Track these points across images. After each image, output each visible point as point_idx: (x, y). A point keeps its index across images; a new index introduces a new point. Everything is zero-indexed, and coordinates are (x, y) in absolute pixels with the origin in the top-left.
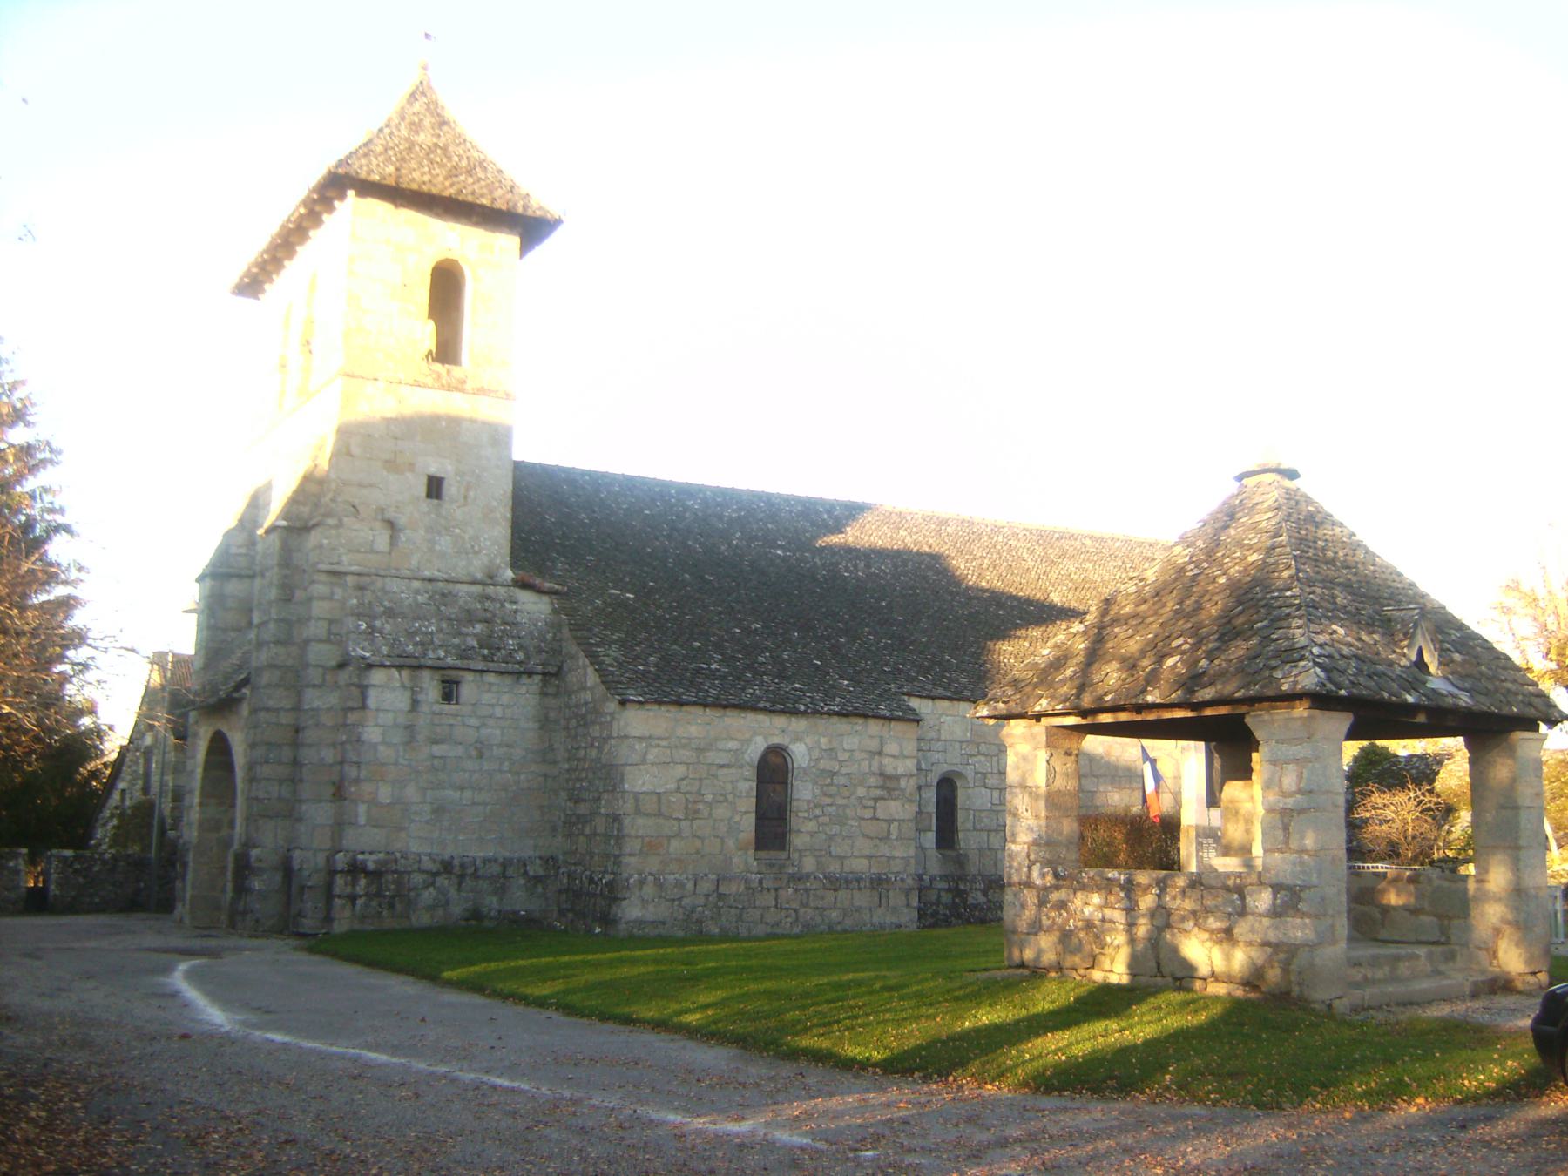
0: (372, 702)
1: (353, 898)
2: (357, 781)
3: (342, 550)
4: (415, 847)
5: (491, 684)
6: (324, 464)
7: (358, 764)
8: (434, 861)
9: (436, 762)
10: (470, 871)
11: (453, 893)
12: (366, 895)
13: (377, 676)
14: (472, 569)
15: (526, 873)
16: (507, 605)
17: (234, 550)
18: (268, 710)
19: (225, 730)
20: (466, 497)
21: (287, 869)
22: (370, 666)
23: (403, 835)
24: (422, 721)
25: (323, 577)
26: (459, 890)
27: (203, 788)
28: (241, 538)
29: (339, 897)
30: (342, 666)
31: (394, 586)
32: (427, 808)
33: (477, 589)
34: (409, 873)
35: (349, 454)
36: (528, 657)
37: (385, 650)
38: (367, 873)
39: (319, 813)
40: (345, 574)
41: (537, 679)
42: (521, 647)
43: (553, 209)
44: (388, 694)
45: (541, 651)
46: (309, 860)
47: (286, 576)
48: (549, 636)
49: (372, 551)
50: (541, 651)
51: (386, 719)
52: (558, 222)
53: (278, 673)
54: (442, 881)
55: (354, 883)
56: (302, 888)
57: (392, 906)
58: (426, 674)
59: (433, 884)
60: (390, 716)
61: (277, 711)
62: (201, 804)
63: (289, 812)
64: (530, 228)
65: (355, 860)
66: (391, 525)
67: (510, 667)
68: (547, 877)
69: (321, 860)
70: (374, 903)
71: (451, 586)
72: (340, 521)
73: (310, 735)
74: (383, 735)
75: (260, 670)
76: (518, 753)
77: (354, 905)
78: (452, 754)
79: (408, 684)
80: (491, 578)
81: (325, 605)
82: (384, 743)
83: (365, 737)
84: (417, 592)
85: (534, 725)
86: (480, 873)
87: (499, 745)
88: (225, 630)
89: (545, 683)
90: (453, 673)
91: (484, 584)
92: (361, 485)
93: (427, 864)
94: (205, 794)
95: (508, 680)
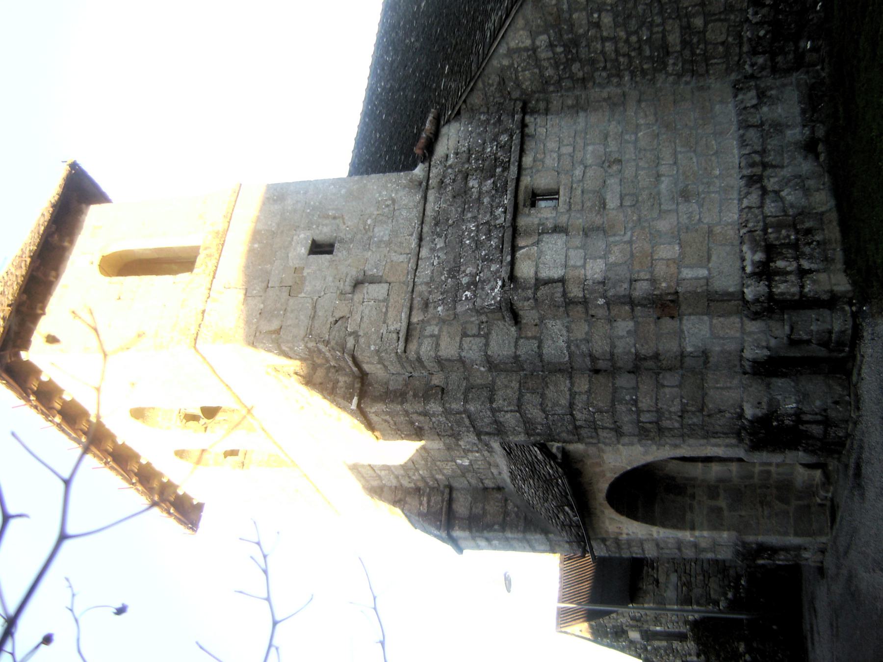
0: (557, 273)
1: (802, 273)
2: (653, 281)
3: (383, 330)
4: (733, 215)
5: (535, 160)
6: (296, 365)
7: (633, 281)
8: (748, 193)
9: (627, 203)
10: (757, 158)
11: (786, 172)
12: (797, 259)
13: (525, 270)
14: (411, 204)
15: (754, 106)
16: (450, 163)
17: (424, 509)
18: (571, 405)
19: (603, 486)
20: (335, 218)
21: (767, 369)
22: (512, 277)
23: (718, 229)
24: (578, 221)
25: (413, 347)
26: (782, 167)
27: (675, 527)
28: (413, 502)
29: (802, 287)
30: (516, 318)
31: (425, 272)
32: (682, 208)
33: (431, 197)
34: (765, 217)
35: (278, 331)
36: (506, 131)
37: (494, 267)
38: (769, 259)
39: (696, 331)
40: (409, 324)
41: (528, 119)
42: (495, 138)
43: (60, 174)
44: (545, 258)
45: (499, 120)
46: (756, 338)
47: (415, 396)
48: (483, 117)
49: (386, 300)
50: (499, 120)
51: (576, 258)
52: (74, 166)
53: (528, 396)
54: (771, 184)
55: (784, 273)
56: (793, 343)
57: (808, 232)
58: (522, 221)
59: (777, 193)
60: (572, 253)
61: (573, 395)
62: (693, 528)
63: (696, 366)
64: (77, 195)
65: (753, 274)
66: (357, 284)
67: (515, 148)
68: (757, 87)
69: (753, 326)
70: (807, 250)
71: (427, 219)
72: (351, 334)
73: (600, 346)
74: (595, 258)
75: (528, 425)
76: (614, 128)
77: (810, 271)
78: (617, 189)
79: (535, 238)
80: (420, 184)
81: (444, 342)
82: (604, 257)
83: (598, 277)
84: (433, 250)
85: (582, 118)
86: (759, 148)
87: (606, 146)
88: (506, 514)
89: (533, 112)
90: (521, 197)
91: (427, 188)
92: (313, 318)
93: (754, 198)
94: (679, 523)
95: (530, 145)
